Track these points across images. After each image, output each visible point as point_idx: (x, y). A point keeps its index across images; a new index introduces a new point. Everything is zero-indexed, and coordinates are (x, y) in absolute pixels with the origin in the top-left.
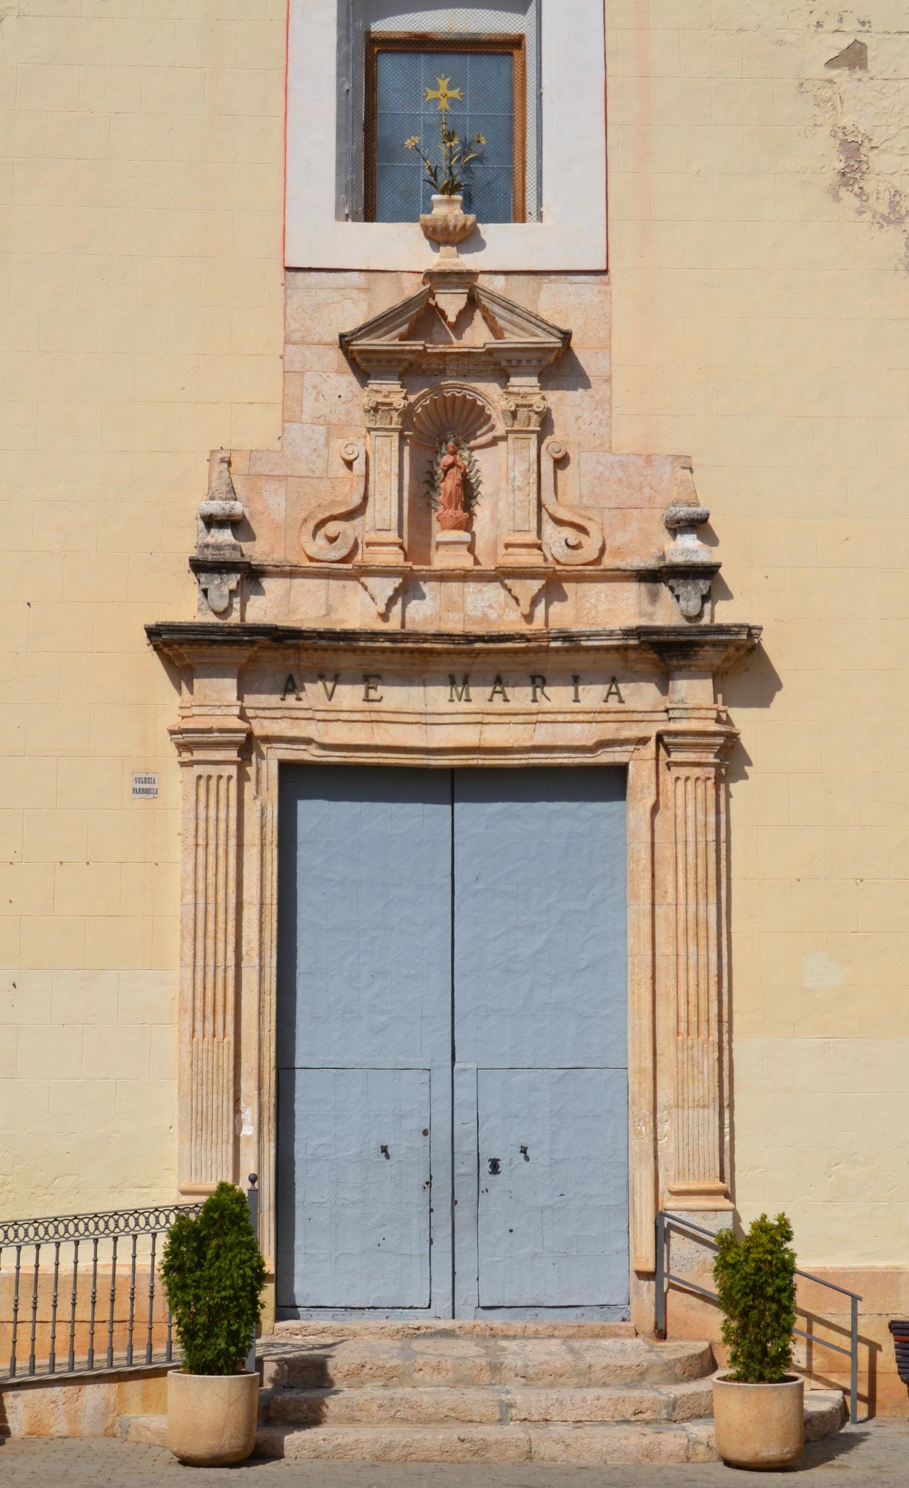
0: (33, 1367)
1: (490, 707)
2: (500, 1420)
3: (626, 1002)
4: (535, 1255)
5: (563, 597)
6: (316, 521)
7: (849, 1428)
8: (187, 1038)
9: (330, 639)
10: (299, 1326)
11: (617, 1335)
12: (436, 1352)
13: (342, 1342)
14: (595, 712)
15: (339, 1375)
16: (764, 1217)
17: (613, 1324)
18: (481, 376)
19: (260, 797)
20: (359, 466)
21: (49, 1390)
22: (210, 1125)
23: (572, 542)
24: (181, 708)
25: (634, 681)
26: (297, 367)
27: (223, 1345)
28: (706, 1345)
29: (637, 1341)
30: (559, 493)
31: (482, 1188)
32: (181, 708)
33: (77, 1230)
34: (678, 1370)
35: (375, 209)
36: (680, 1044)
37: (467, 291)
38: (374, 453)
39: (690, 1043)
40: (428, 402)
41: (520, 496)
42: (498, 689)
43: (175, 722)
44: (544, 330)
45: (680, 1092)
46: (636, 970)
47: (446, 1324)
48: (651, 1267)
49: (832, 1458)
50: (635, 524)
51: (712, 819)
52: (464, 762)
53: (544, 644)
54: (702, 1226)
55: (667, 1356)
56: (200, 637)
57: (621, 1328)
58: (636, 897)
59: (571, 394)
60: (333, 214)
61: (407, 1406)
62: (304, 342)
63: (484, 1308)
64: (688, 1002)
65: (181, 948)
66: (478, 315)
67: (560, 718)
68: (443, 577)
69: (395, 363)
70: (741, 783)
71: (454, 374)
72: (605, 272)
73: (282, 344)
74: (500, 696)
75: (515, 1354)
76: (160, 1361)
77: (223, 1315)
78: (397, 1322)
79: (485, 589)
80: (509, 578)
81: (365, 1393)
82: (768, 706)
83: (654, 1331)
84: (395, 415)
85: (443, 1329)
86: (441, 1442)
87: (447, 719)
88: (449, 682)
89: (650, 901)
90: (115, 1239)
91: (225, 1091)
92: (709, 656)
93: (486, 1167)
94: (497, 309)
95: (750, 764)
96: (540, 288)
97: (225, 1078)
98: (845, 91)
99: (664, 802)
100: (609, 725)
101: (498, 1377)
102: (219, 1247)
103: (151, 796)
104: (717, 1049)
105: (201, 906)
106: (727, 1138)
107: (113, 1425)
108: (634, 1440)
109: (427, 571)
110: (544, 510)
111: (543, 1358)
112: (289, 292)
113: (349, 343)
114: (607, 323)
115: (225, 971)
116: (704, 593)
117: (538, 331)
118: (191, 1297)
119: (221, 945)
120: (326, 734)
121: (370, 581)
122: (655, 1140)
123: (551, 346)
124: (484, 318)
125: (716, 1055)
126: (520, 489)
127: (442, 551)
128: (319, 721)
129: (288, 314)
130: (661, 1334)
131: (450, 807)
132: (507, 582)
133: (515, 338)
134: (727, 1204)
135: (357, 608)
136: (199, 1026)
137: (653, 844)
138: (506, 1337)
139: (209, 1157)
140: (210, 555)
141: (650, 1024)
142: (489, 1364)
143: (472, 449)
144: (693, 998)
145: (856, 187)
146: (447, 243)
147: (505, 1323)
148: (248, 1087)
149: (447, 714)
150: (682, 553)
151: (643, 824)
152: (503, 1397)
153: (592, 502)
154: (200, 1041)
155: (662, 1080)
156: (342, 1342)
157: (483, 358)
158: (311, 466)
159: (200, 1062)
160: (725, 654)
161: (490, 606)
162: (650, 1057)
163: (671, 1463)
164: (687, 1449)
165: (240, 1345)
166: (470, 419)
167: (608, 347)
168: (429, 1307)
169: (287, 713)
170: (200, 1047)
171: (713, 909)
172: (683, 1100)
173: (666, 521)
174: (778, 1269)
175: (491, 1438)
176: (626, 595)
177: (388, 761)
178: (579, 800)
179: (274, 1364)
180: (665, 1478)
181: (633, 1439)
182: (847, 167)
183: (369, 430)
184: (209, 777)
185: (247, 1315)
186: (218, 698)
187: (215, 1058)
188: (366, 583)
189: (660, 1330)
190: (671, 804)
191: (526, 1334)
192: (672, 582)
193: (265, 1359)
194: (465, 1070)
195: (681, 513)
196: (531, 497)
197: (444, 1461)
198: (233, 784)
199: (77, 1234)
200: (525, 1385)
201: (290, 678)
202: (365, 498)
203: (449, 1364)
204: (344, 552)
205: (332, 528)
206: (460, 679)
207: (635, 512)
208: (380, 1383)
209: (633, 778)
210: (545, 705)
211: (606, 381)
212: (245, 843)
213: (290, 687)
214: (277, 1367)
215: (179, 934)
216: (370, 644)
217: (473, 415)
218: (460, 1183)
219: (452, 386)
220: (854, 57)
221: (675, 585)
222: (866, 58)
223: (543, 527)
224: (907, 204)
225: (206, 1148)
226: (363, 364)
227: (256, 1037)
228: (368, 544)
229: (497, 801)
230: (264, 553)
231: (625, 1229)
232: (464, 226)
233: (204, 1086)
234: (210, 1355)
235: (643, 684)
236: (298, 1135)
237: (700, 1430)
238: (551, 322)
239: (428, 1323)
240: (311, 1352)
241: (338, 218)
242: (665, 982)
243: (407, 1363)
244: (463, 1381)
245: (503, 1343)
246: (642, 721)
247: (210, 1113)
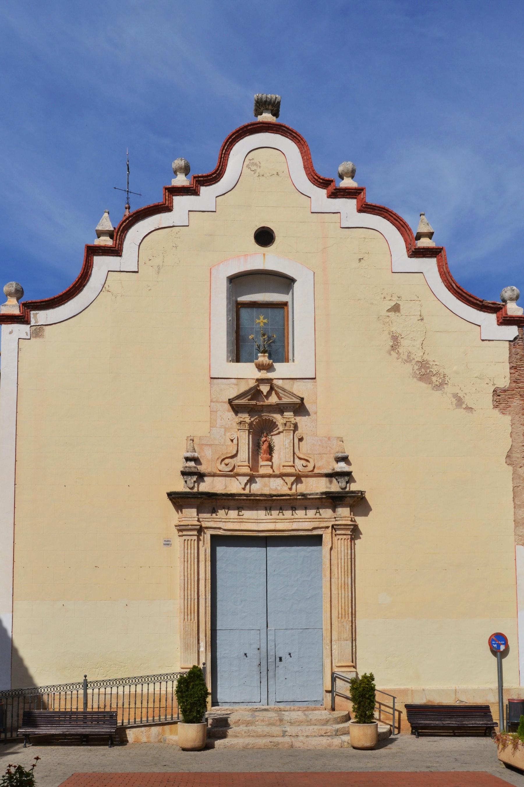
4: (293, 686)
5: (301, 482)
7: (392, 736)
8: (182, 621)
11: (319, 710)
16: (365, 674)
18: (275, 412)
20: (235, 441)
23: (304, 465)
26: (215, 410)
28: (347, 712)
34: (339, 720)
41: (287, 450)
47: (266, 707)
48: (330, 689)
49: (386, 746)
51: (349, 552)
55: (335, 716)
59: (304, 418)
66: (273, 392)
67: (301, 520)
68: (263, 476)
70: (359, 540)
72: (315, 378)
76: (175, 719)
78: (250, 707)
87: (264, 521)
92: (348, 500)
93: (278, 659)
94: (280, 391)
99: (335, 546)
102: (193, 685)
105: (186, 580)
108: (325, 741)
111: (296, 717)
113: (231, 402)
117: (293, 398)
119: (193, 592)
122: (331, 650)
126: (287, 448)
127: (262, 468)
130: (333, 709)
133: (286, 400)
134: (354, 670)
135: (235, 486)
136: (186, 617)
137: (331, 559)
138: (284, 711)
140: (187, 470)
143: (272, 435)
146: (263, 369)
152: (284, 729)
161: (278, 485)
169: (213, 520)
171: (350, 579)
175: (280, 741)
181: (325, 741)
183: (238, 430)
186: (190, 515)
190: (336, 547)
192: (336, 477)
198: (196, 542)
201: (214, 509)
202: (237, 451)
204: (231, 469)
205: (227, 461)
206: (268, 508)
210: (296, 516)
218: (269, 664)
219: (265, 415)
220: (396, 308)
224: (413, 356)
226: (236, 409)
228: (239, 466)
234: (191, 717)
237: (345, 738)
242: (334, 602)
245: (283, 713)
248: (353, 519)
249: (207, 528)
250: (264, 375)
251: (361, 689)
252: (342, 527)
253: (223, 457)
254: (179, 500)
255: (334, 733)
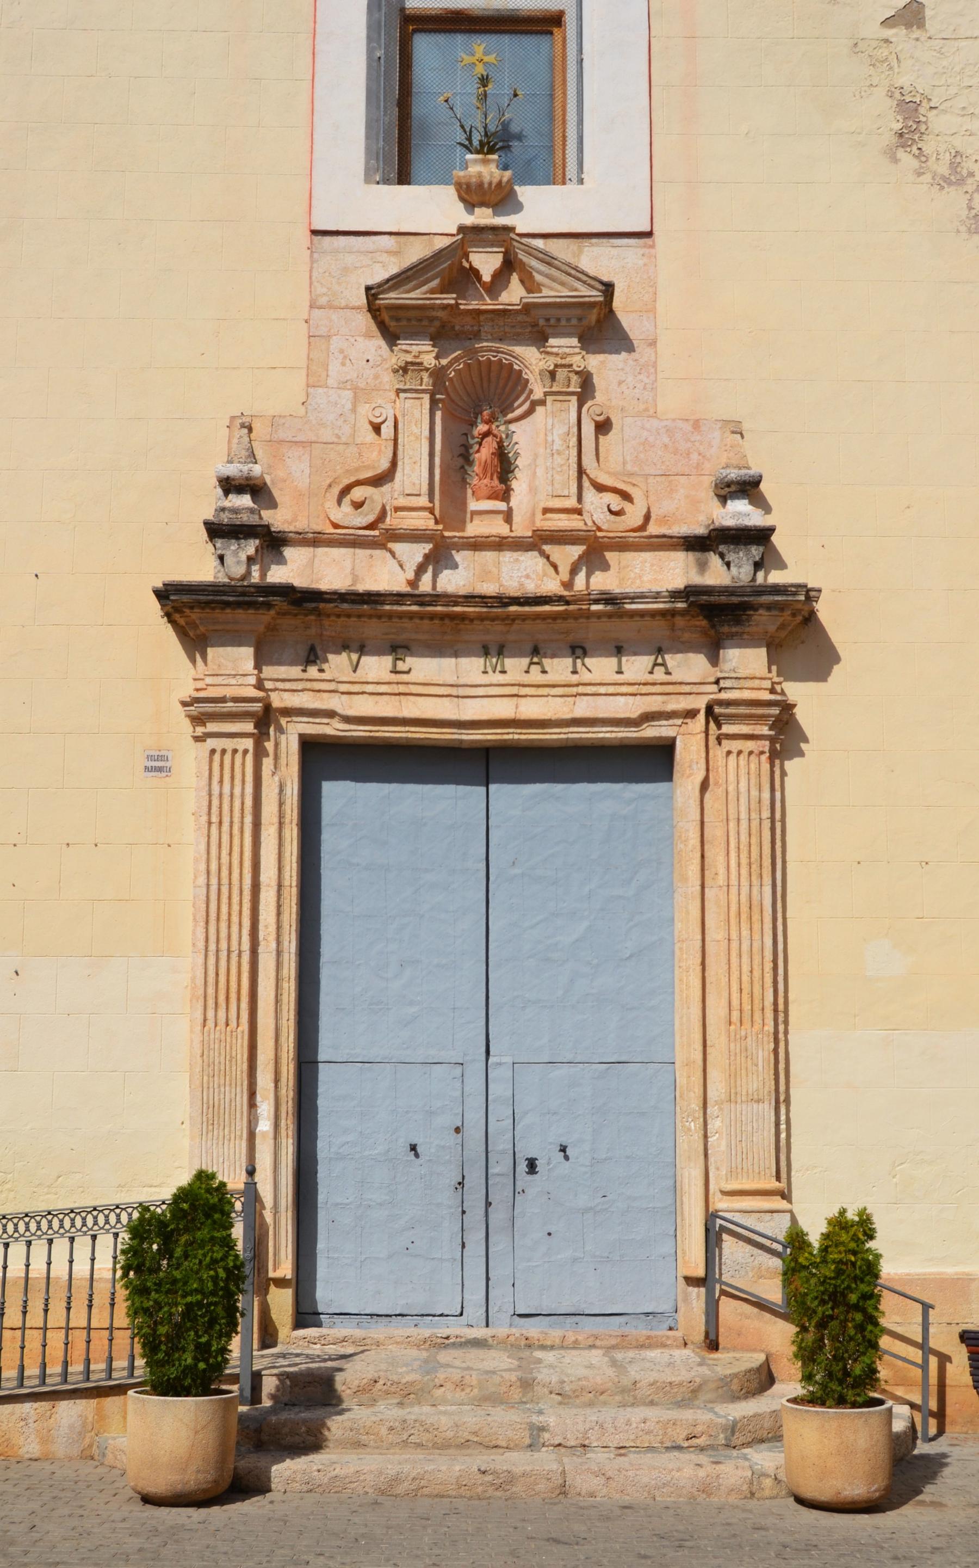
0: (43, 1376)
1: (527, 679)
2: (530, 1446)
3: (673, 993)
4: (575, 1260)
5: (605, 567)
6: (341, 486)
7: (922, 1448)
8: (198, 1028)
9: (353, 602)
10: (317, 1335)
11: (664, 1346)
12: (464, 1365)
13: (362, 1352)
14: (639, 684)
15: (348, 1391)
16: (843, 1212)
17: (659, 1333)
18: (518, 339)
19: (279, 773)
20: (387, 430)
21: (18, 1406)
22: (222, 1119)
23: (615, 508)
24: (195, 680)
25: (682, 652)
26: (323, 331)
27: (189, 1361)
28: (762, 1357)
29: (687, 1352)
30: (601, 459)
31: (519, 1189)
32: (195, 680)
33: (50, 1227)
34: (735, 1386)
35: (409, 174)
36: (732, 1034)
37: (503, 250)
38: (404, 416)
39: (743, 1033)
40: (461, 366)
41: (559, 460)
42: (535, 660)
43: (187, 692)
44: (584, 282)
45: (733, 1085)
46: (685, 956)
47: (479, 1332)
48: (701, 1272)
49: (919, 1492)
50: (682, 491)
51: (766, 795)
52: (499, 737)
53: (584, 607)
54: (757, 1229)
55: (722, 1371)
56: (211, 597)
57: (668, 1337)
58: (685, 879)
59: (614, 357)
60: (363, 177)
61: (422, 1429)
62: (331, 306)
63: (520, 1316)
64: (741, 990)
65: (194, 933)
66: (515, 278)
67: (602, 690)
68: (477, 545)
69: (425, 323)
70: (797, 760)
71: (490, 337)
72: (649, 234)
73: (307, 308)
74: (538, 668)
75: (554, 1367)
76: (120, 1376)
77: (188, 1325)
78: (425, 1331)
79: (522, 558)
80: (547, 544)
81: (375, 1414)
82: (825, 680)
83: (705, 1341)
84: (425, 375)
85: (475, 1338)
86: (458, 1474)
87: (481, 691)
88: (482, 653)
89: (699, 883)
90: (94, 1237)
91: (239, 1083)
92: (763, 621)
93: (522, 1167)
94: (534, 263)
95: (806, 740)
96: (581, 251)
97: (239, 1069)
98: (901, 51)
99: (715, 777)
100: (655, 697)
101: (530, 1394)
102: (190, 1244)
103: (164, 774)
104: (772, 1040)
105: (214, 888)
106: (783, 1136)
107: (90, 1446)
108: (688, 1471)
109: (459, 537)
110: (584, 477)
111: (582, 1372)
112: (315, 255)
113: (375, 296)
114: (651, 286)
115: (240, 956)
116: (757, 559)
117: (578, 285)
118: (151, 1303)
119: (235, 928)
120: (351, 707)
121: (397, 547)
122: (706, 1136)
123: (592, 299)
124: (522, 281)
125: (772, 1046)
126: (559, 453)
127: (477, 520)
128: (343, 693)
129: (314, 278)
130: (713, 1345)
131: (485, 788)
132: (545, 547)
133: (552, 292)
134: (783, 1205)
135: (385, 573)
136: (211, 1014)
137: (702, 823)
138: (543, 1347)
139: (221, 1153)
140: (225, 518)
141: (700, 1013)
142: (520, 1379)
143: (510, 422)
144: (746, 986)
145: (914, 148)
146: (483, 204)
147: (542, 1332)
148: (264, 1080)
149: (480, 686)
150: (733, 517)
151: (691, 801)
152: (535, 1419)
153: (636, 469)
154: (212, 1031)
155: (712, 1074)
156: (362, 1352)
157: (520, 318)
158: (336, 432)
159: (212, 1052)
160: (781, 619)
161: (528, 577)
162: (699, 1048)
163: (733, 1499)
164: (751, 1483)
165: (211, 1361)
166: (507, 389)
167: (653, 310)
168: (461, 1314)
169: (309, 685)
170: (212, 1036)
171: (768, 890)
172: (736, 1093)
173: (716, 485)
174: (863, 1272)
175: (518, 1470)
176: (672, 564)
177: (417, 736)
178: (622, 782)
179: (274, 1378)
180: (728, 1524)
181: (686, 1470)
182: (906, 127)
183: (399, 391)
184: (224, 752)
185: (220, 1324)
187: (228, 1048)
188: (393, 549)
189: (711, 1341)
190: (722, 781)
191: (565, 1344)
192: (722, 548)
193: (263, 1373)
194: (500, 1064)
195: (732, 475)
196: (570, 461)
197: (462, 1497)
198: (250, 758)
199: (50, 1232)
200: (560, 1403)
201: (312, 649)
202: (394, 463)
203: (473, 1379)
204: (371, 518)
205: (358, 493)
206: (494, 650)
207: (683, 479)
208: (396, 1401)
209: (680, 753)
210: (585, 676)
211: (650, 345)
212: (263, 821)
213: (312, 658)
214: (277, 1382)
215: (191, 917)
216: (395, 608)
217: (510, 384)
218: (493, 1184)
219: (488, 349)
221: (725, 551)
222: (924, 18)
223: (584, 494)
224: (968, 165)
225: (217, 1144)
227: (273, 1026)
228: (397, 509)
229: (535, 782)
230: (286, 521)
231: (672, 1233)
232: (500, 182)
233: (216, 1078)
234: (173, 1372)
235: (691, 655)
236: (320, 1133)
237: (765, 1459)
238: (591, 273)
239: (458, 1331)
240: (322, 1365)
241: (368, 180)
242: (716, 970)
243: (426, 1379)
244: (491, 1399)
245: (539, 1354)
246: (690, 694)
247: (222, 1107)
248: (778, 688)
249: (288, 712)
250: (483, 217)
251: (829, 1270)
252: (742, 710)
253: (346, 481)
254: (195, 615)
255: (721, 1439)
